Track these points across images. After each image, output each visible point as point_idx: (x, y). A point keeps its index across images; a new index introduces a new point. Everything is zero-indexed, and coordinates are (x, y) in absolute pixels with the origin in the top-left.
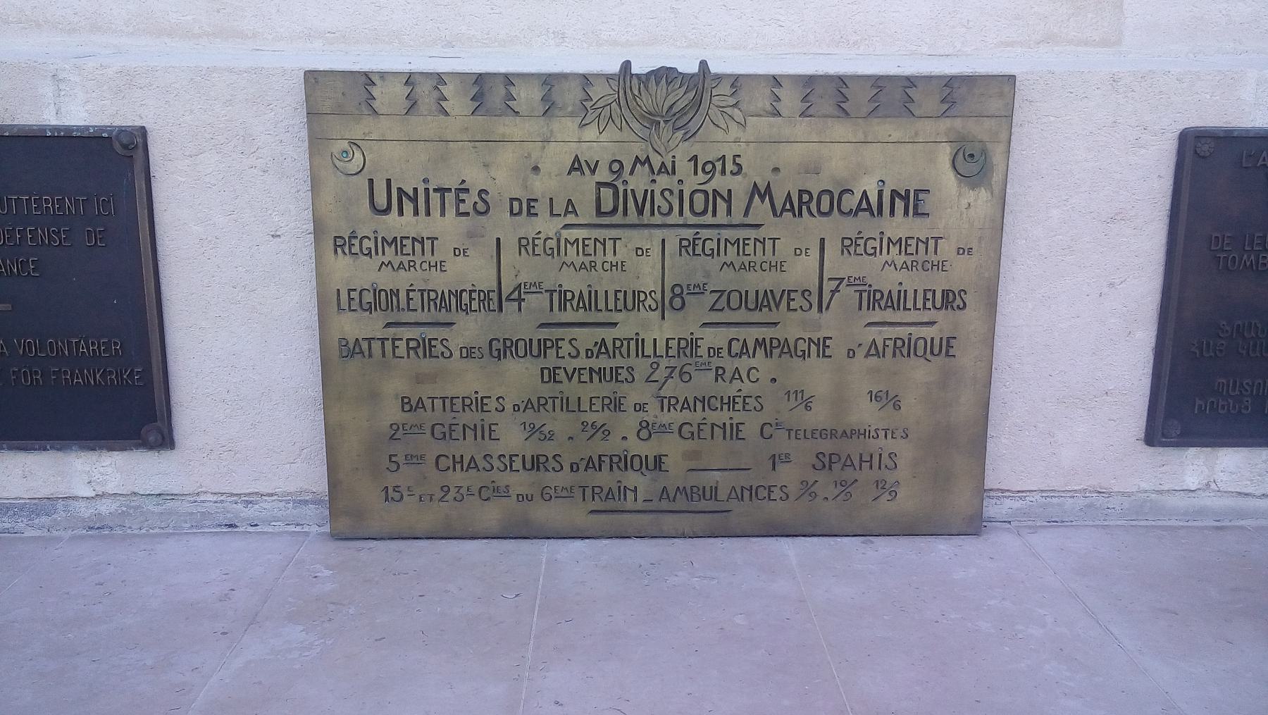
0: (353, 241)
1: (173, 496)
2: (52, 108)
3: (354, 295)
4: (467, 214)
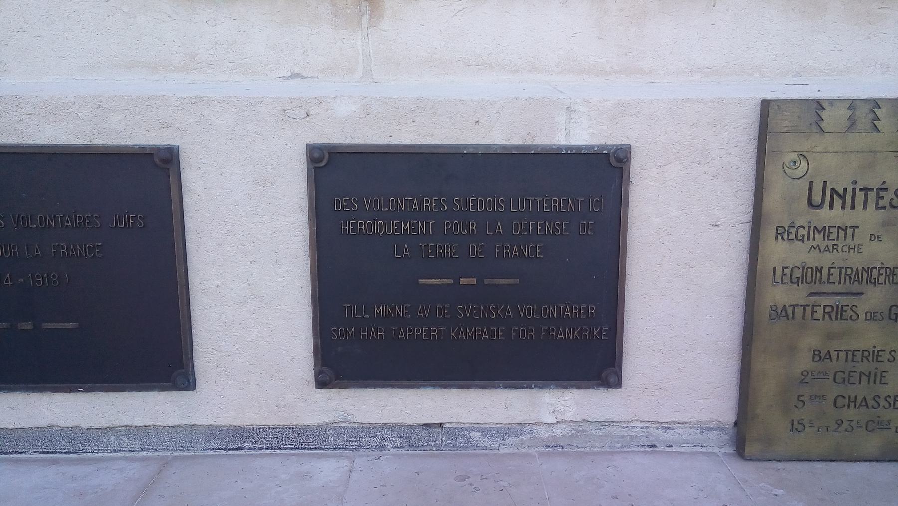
0: (792, 230)
1: (610, 423)
2: (564, 132)
3: (787, 271)
4: (883, 208)
